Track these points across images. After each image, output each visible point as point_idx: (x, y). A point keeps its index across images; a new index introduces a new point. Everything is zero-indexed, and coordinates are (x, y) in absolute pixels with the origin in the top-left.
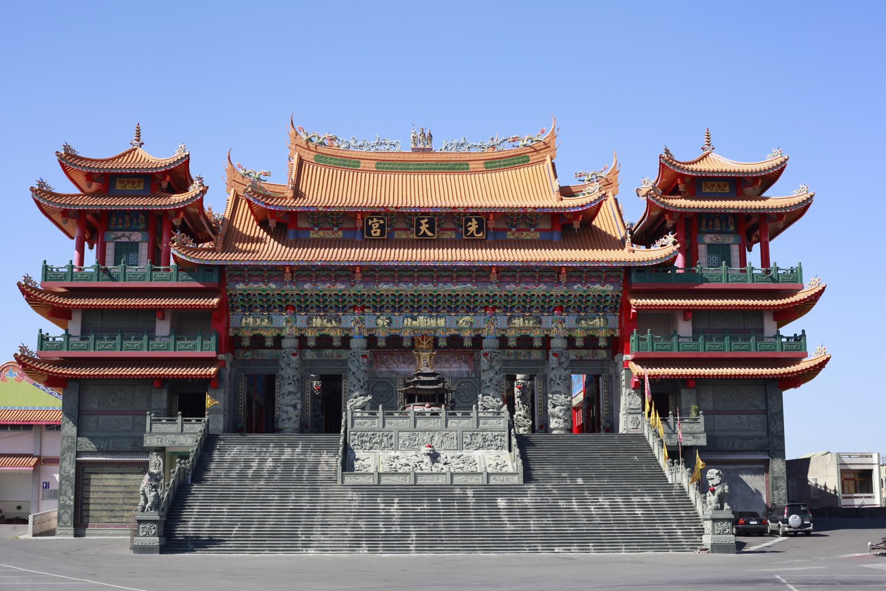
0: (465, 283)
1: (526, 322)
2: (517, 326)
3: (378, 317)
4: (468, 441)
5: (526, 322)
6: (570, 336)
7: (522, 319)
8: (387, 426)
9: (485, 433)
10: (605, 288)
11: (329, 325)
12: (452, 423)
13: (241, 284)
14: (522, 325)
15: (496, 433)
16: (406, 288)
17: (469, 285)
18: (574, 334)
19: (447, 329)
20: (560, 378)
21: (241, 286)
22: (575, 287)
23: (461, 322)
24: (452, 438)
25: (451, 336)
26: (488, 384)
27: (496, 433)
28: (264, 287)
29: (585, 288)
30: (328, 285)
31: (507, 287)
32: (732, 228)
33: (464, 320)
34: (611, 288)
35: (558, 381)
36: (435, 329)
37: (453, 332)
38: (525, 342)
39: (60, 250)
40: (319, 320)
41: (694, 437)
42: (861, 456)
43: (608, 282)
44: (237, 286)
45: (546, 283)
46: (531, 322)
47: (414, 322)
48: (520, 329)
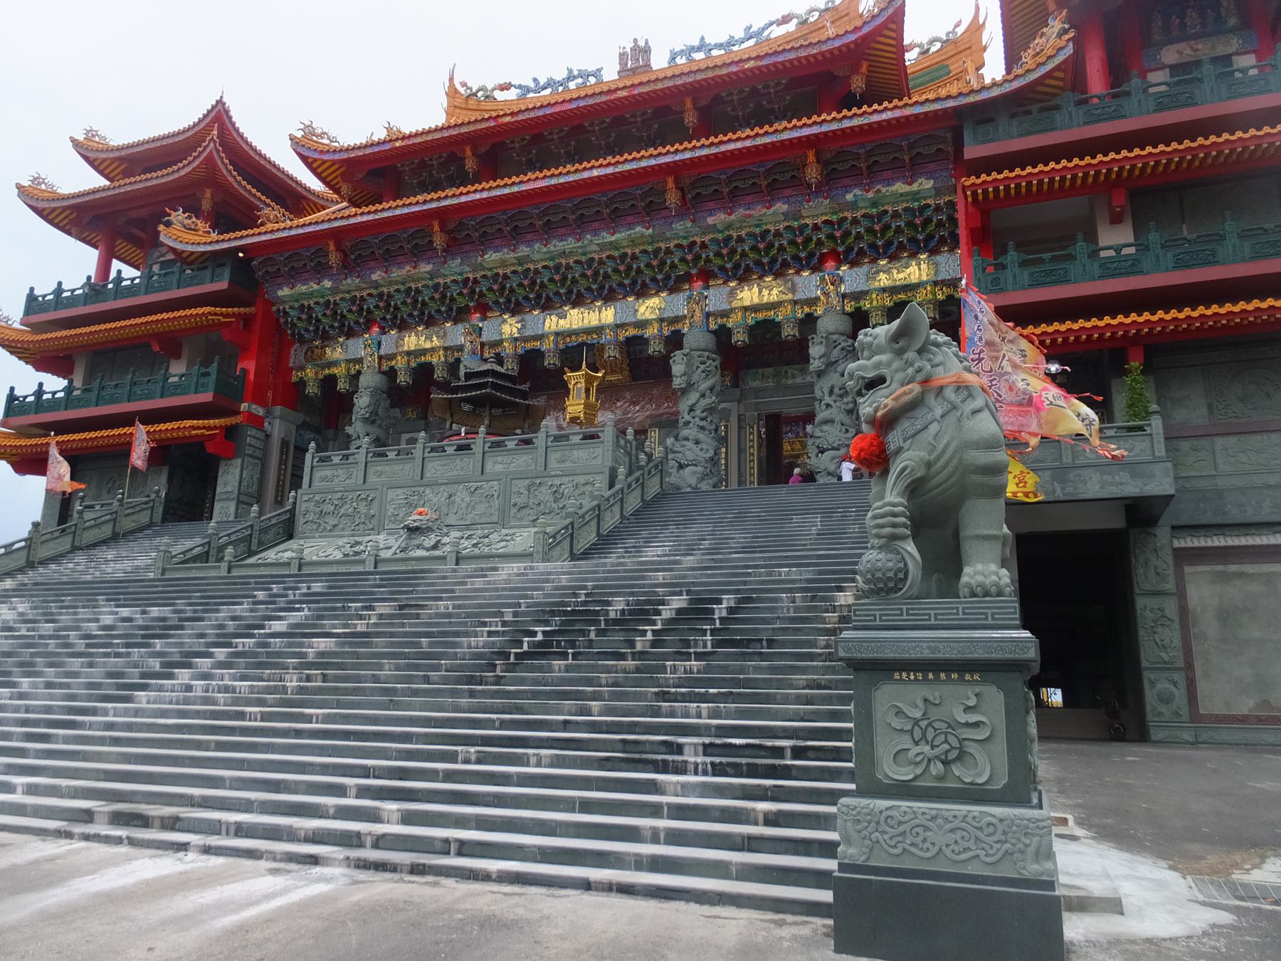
0: (630, 226)
1: (765, 292)
2: (747, 303)
3: (505, 321)
4: (521, 501)
5: (765, 292)
6: (858, 309)
7: (756, 289)
8: (372, 478)
9: (557, 481)
10: (915, 187)
11: (428, 345)
12: (496, 464)
13: (286, 289)
14: (756, 300)
15: (581, 479)
16: (537, 253)
17: (638, 229)
18: (866, 305)
19: (619, 326)
20: (831, 392)
21: (284, 292)
22: (849, 197)
23: (642, 309)
24: (489, 497)
25: (628, 339)
26: (687, 417)
27: (581, 479)
28: (316, 287)
29: (870, 195)
30: (408, 268)
31: (710, 220)
32: (1233, 21)
33: (649, 308)
34: (928, 184)
35: (828, 399)
36: (599, 330)
37: (631, 332)
38: (764, 332)
39: (71, 264)
40: (413, 338)
41: (1134, 475)
42: (1078, 853)
43: (921, 175)
44: (280, 293)
45: (787, 199)
46: (775, 291)
47: (562, 322)
48: (755, 309)
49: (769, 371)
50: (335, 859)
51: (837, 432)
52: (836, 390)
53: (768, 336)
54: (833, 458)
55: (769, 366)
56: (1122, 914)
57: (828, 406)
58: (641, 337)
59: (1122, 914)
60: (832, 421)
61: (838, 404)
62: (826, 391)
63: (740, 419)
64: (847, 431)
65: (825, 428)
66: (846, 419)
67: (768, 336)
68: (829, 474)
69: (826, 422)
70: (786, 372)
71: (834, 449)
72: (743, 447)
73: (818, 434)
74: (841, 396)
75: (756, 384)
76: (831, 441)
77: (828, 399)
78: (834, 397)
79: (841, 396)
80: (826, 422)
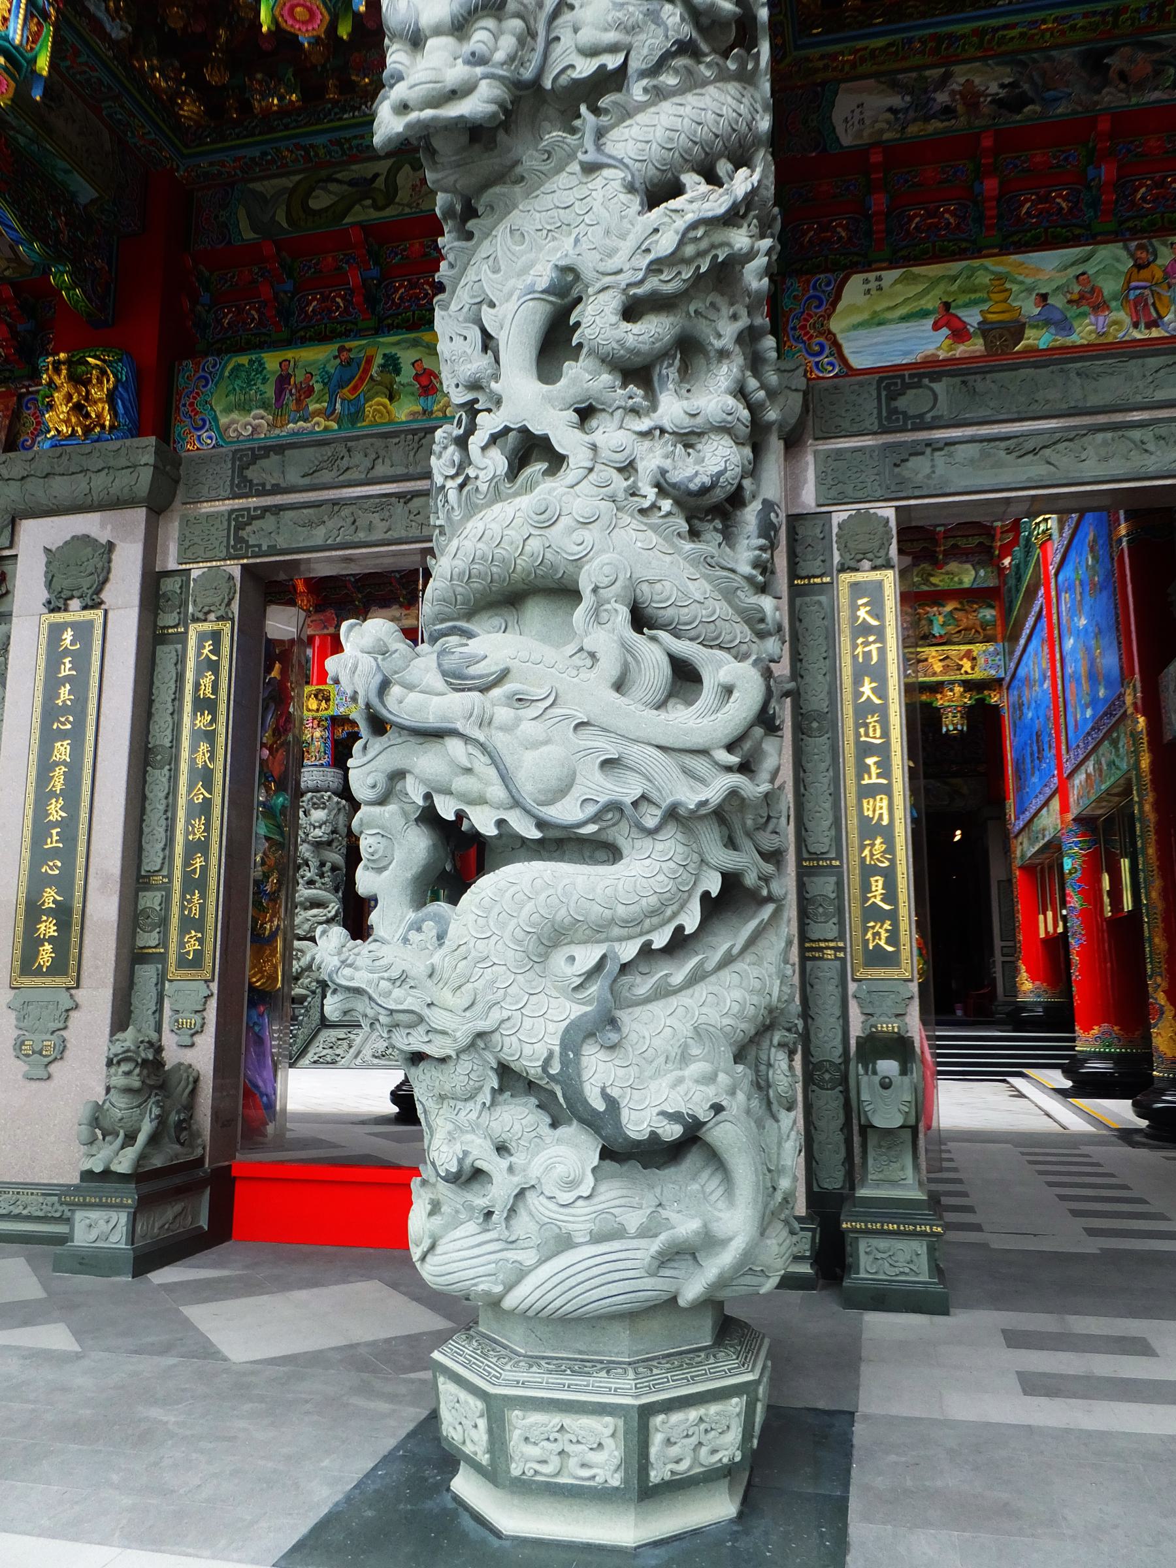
20: (556, 343)
35: (527, 398)
49: (315, 357)
50: (1036, 327)
51: (591, 692)
52: (598, 320)
53: (320, 201)
54: (554, 937)
55: (322, 338)
56: (1004, 1331)
57: (530, 450)
58: (1049, 843)
59: (1004, 1331)
60: (563, 591)
61: (611, 434)
62: (518, 325)
63: (155, 592)
64: (685, 676)
65: (493, 644)
66: (677, 571)
67: (320, 201)
68: (509, 1079)
69: (518, 593)
70: (392, 365)
71: (558, 843)
72: (161, 736)
73: (422, 695)
74: (637, 372)
75: (244, 424)
76: (533, 768)
77: (527, 398)
78: (581, 376)
79: (637, 372)
80: (518, 593)
